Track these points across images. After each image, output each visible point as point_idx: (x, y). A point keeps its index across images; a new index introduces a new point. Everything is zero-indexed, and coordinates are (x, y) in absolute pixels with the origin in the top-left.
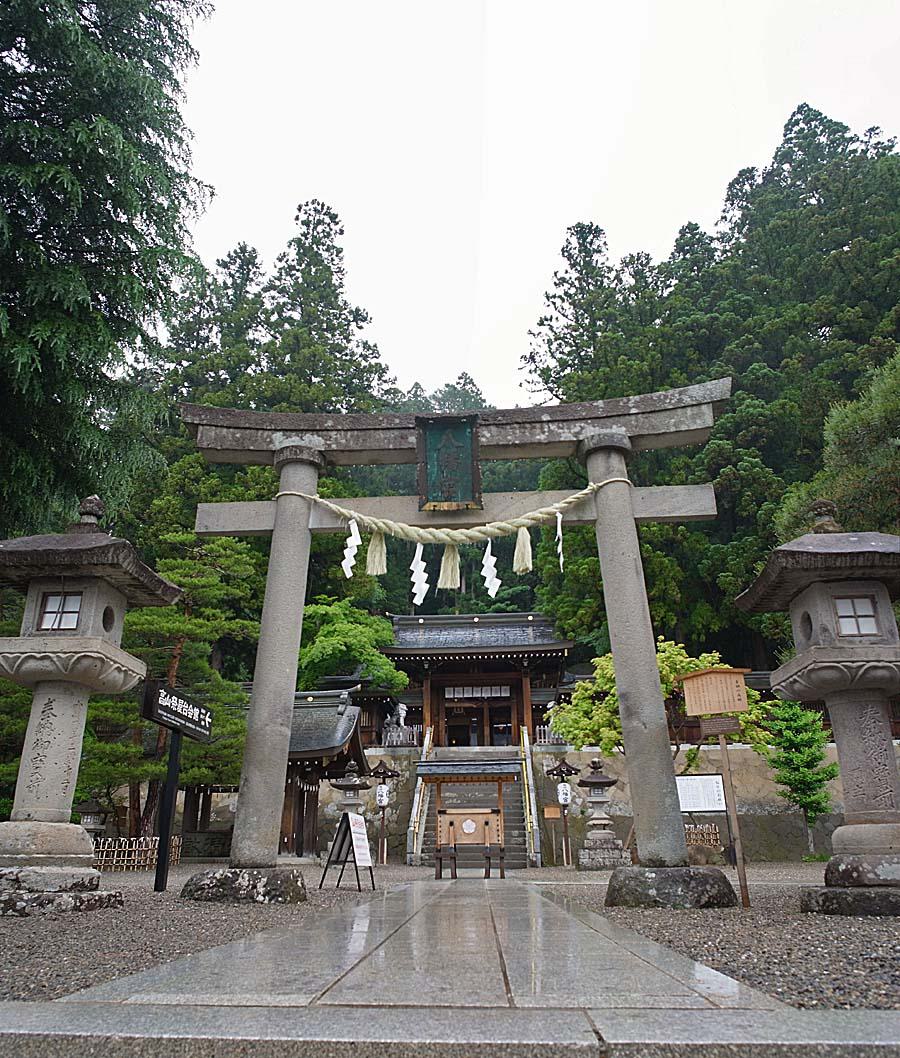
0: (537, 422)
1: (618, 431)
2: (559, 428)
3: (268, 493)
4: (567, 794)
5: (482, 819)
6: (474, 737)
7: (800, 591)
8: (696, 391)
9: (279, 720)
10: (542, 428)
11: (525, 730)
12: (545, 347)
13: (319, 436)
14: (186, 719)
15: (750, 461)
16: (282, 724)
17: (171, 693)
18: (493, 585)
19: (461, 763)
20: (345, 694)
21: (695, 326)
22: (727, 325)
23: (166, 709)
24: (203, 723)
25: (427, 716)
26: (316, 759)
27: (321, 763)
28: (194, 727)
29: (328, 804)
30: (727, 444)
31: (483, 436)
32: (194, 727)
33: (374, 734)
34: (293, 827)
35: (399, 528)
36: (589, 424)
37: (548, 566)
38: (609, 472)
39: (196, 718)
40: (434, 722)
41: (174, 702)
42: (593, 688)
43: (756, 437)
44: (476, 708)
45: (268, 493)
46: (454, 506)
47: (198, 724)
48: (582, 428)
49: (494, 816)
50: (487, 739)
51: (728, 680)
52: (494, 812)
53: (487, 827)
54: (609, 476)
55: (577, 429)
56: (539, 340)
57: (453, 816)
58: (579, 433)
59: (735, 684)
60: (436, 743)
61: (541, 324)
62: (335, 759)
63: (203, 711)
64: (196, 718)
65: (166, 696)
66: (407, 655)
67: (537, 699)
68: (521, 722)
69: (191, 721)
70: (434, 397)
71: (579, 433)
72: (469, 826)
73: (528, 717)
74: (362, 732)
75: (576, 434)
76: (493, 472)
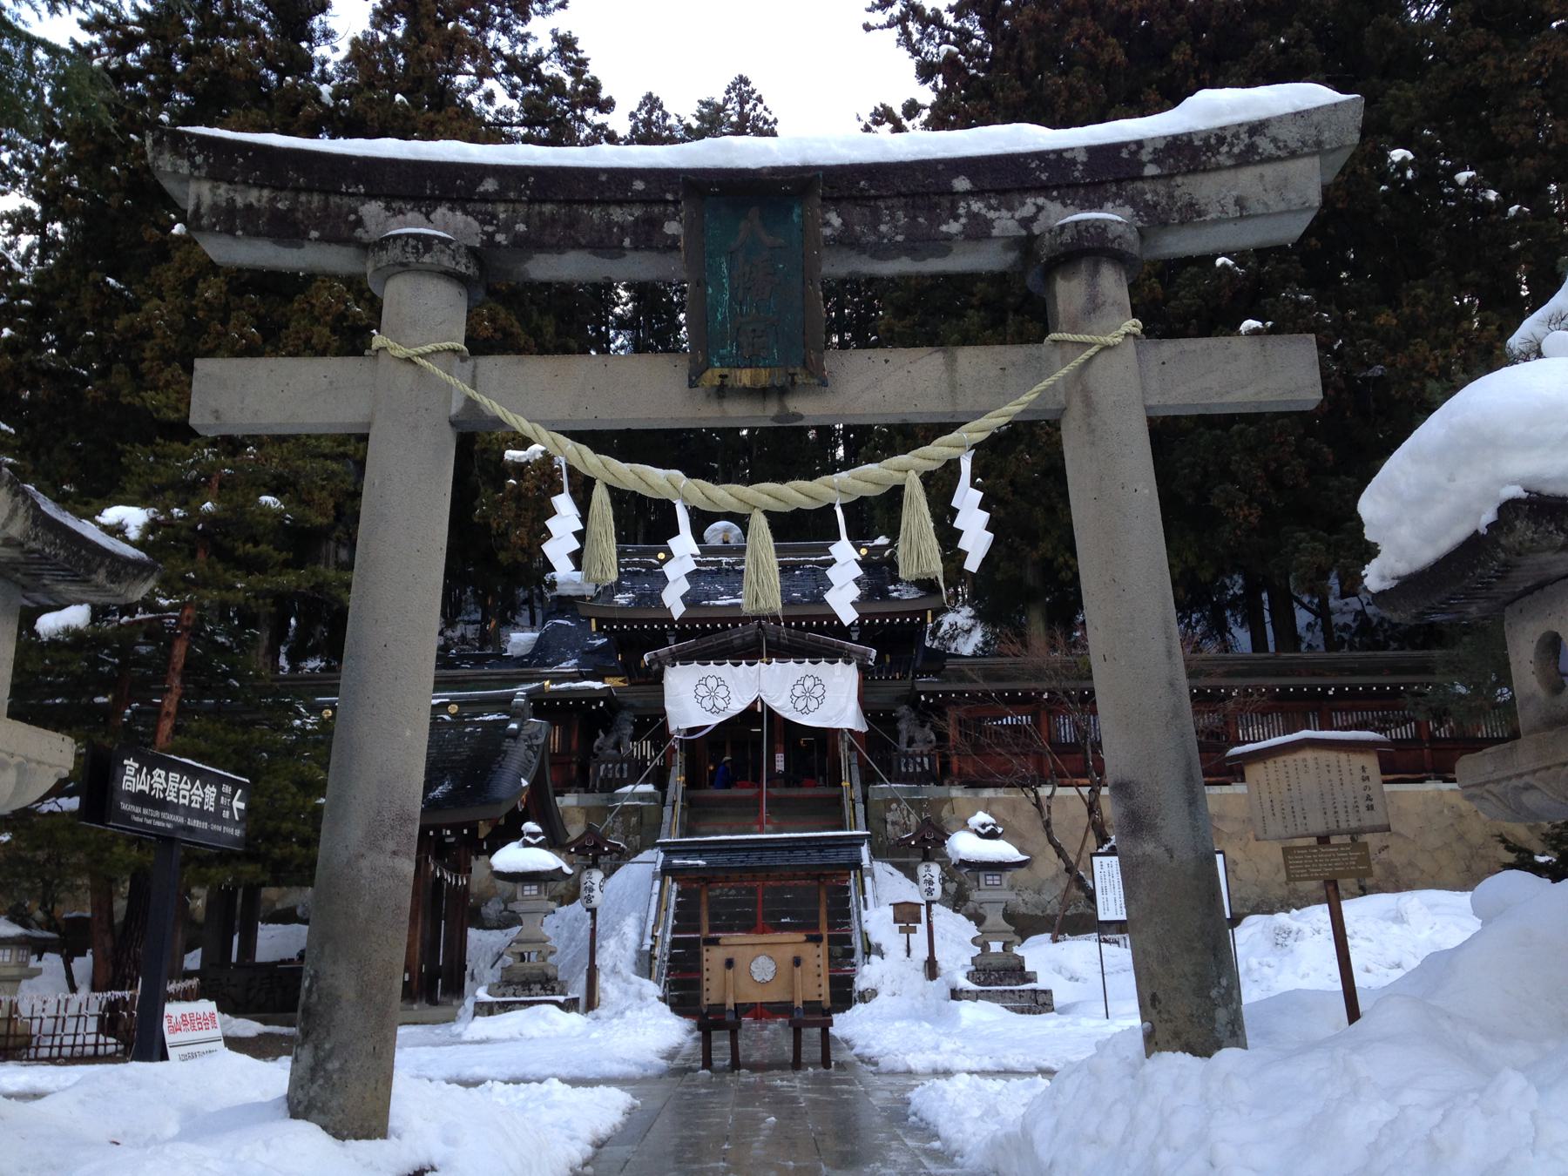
0: (942, 194)
2: (990, 207)
3: (352, 335)
4: (931, 882)
5: (789, 953)
7: (1540, 586)
9: (390, 845)
10: (954, 207)
13: (466, 213)
14: (189, 811)
16: (395, 853)
17: (150, 763)
23: (141, 798)
24: (226, 814)
26: (464, 825)
27: (474, 830)
28: (205, 825)
29: (489, 899)
31: (827, 224)
32: (205, 825)
33: (574, 767)
34: (422, 955)
36: (1053, 199)
37: (273, 77)
38: (1094, 306)
39: (210, 806)
41: (162, 782)
45: (352, 335)
46: (764, 377)
47: (216, 817)
48: (1040, 209)
49: (811, 947)
52: (810, 939)
53: (798, 971)
54: (1100, 325)
55: (1028, 210)
57: (732, 949)
58: (1033, 219)
59: (1358, 774)
62: (502, 822)
63: (227, 789)
64: (210, 806)
65: (139, 771)
66: (635, 621)
69: (202, 814)
71: (1033, 219)
72: (763, 968)
74: (552, 764)
75: (1026, 223)
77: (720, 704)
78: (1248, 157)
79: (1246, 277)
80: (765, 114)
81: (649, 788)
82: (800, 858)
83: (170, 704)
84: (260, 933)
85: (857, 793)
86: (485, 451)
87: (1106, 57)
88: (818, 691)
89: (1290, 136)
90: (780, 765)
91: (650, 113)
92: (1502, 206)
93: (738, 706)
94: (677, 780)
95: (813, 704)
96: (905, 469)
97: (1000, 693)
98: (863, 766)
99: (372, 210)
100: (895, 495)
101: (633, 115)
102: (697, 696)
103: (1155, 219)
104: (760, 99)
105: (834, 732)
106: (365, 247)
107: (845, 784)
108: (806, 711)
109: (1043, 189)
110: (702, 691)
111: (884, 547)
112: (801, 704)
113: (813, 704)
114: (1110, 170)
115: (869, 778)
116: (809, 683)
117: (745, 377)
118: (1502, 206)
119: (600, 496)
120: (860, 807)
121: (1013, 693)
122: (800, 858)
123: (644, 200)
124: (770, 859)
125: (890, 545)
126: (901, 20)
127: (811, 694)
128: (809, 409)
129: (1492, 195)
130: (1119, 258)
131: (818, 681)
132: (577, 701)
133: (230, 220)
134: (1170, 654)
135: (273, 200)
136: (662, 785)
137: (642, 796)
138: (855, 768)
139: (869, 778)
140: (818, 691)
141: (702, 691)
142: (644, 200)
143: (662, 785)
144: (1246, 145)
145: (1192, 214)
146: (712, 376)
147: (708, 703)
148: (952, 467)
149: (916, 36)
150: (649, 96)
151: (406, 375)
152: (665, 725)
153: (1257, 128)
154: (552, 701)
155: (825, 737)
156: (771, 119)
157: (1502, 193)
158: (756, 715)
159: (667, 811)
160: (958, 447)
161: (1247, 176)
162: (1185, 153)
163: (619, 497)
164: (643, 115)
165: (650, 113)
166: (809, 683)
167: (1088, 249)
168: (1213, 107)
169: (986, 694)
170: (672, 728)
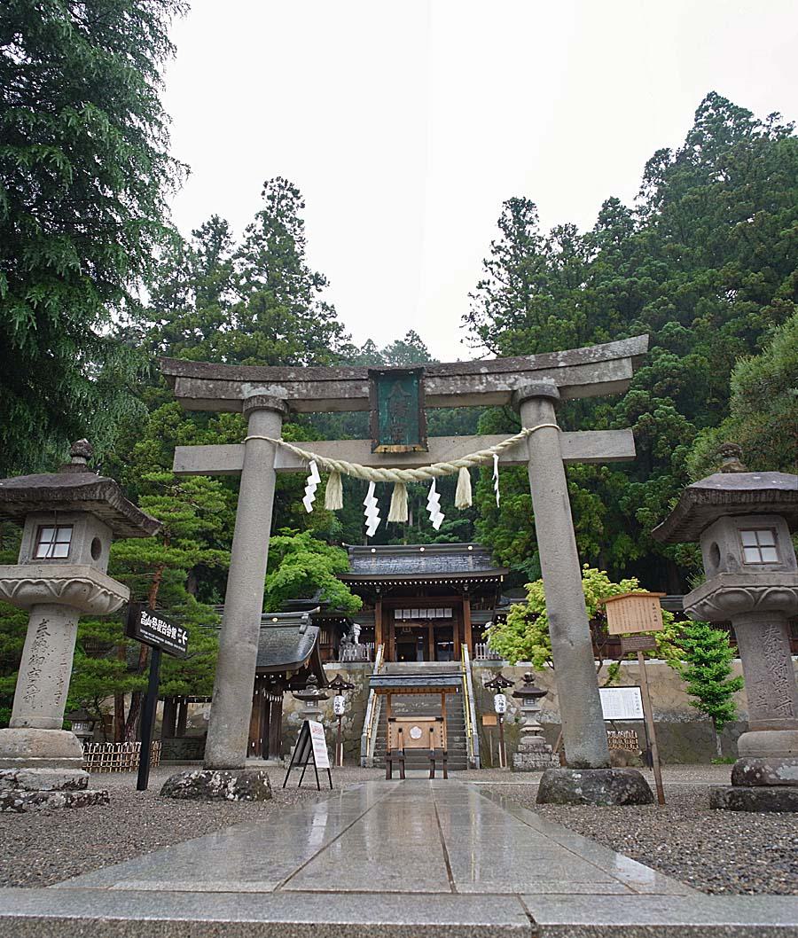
0: (476, 374)
1: (548, 382)
2: (496, 379)
3: (238, 437)
4: (502, 704)
5: (427, 726)
6: (420, 654)
8: (617, 347)
9: (248, 639)
10: (480, 380)
11: (465, 647)
12: (484, 308)
13: (283, 386)
14: (165, 637)
15: (665, 408)
16: (250, 642)
17: (151, 614)
18: (437, 519)
19: (409, 676)
20: (306, 615)
21: (616, 289)
22: (644, 288)
23: (147, 628)
24: (180, 641)
25: (379, 635)
26: (280, 673)
27: (284, 676)
28: (172, 644)
29: (291, 713)
30: (644, 394)
31: (429, 387)
32: (172, 644)
33: (332, 650)
34: (260, 733)
35: (354, 468)
36: (522, 376)
38: (540, 418)
39: (174, 637)
40: (385, 640)
41: (154, 623)
42: (525, 610)
43: (670, 388)
44: (422, 628)
45: (238, 437)
46: (402, 448)
47: (175, 642)
48: (516, 380)
49: (438, 724)
50: (432, 655)
51: (646, 603)
52: (438, 720)
53: (432, 734)
54: (540, 422)
55: (512, 380)
56: (478, 301)
57: (402, 724)
58: (513, 384)
60: (387, 658)
61: (480, 287)
62: (297, 673)
63: (180, 630)
64: (174, 637)
65: (147, 617)
66: (361, 581)
67: (476, 620)
68: (462, 640)
69: (170, 639)
70: (385, 352)
71: (513, 384)
72: (416, 733)
73: (468, 636)
74: (321, 649)
75: (511, 385)
76: (437, 419)
134: (571, 541)
135: (159, 721)
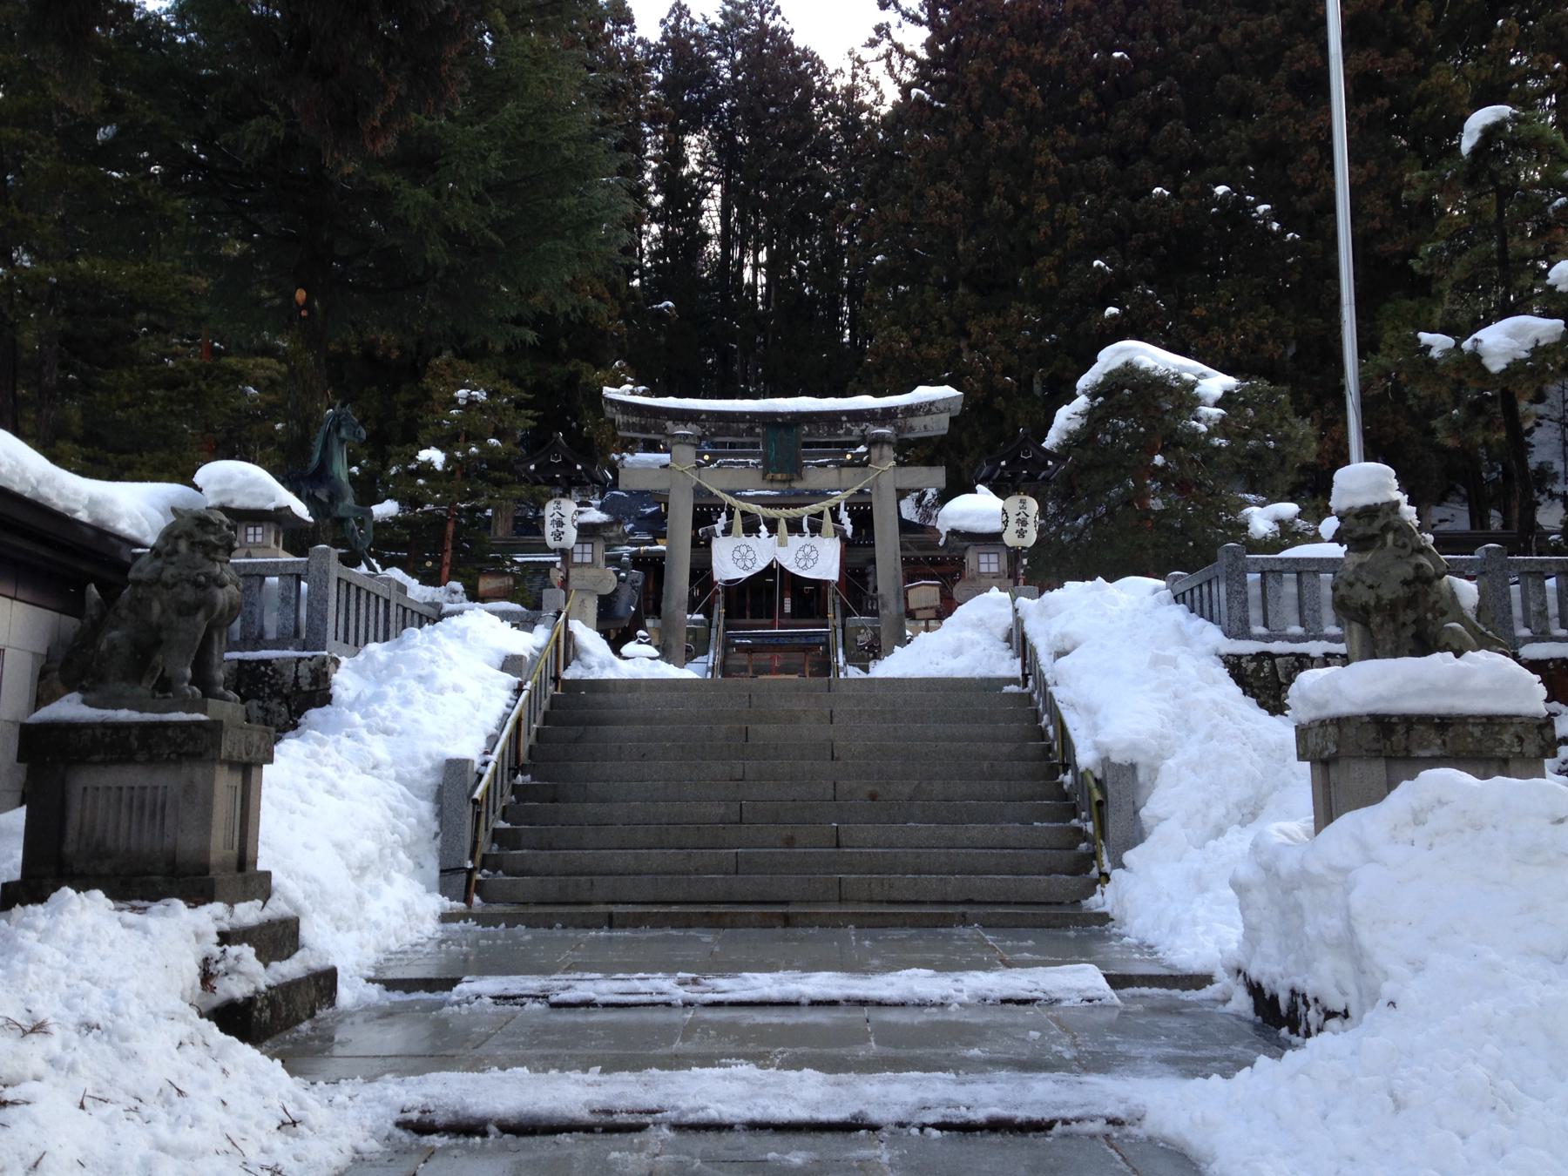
38: (881, 458)
54: (886, 462)
77: (749, 564)
78: (929, 412)
79: (1112, 275)
80: (783, 24)
81: (701, 617)
82: (796, 640)
83: (447, 558)
84: (836, 566)
85: (838, 621)
86: (586, 384)
87: (1029, 101)
88: (814, 555)
89: (941, 407)
90: (788, 609)
91: (678, 19)
92: (1282, 233)
93: (761, 565)
94: (719, 610)
95: (810, 564)
96: (824, 506)
97: (926, 558)
98: (843, 604)
99: (669, 424)
100: (820, 515)
101: (663, 22)
102: (735, 559)
103: (899, 430)
104: (778, 11)
105: (826, 582)
106: (668, 436)
107: (830, 616)
108: (805, 568)
109: (868, 421)
110: (737, 555)
111: (863, 454)
112: (802, 564)
113: (810, 564)
114: (887, 415)
115: (846, 613)
116: (807, 550)
117: (779, 476)
118: (1282, 233)
119: (737, 514)
120: (839, 631)
121: (934, 558)
122: (796, 640)
123: (749, 421)
124: (781, 640)
125: (868, 453)
126: (888, 56)
127: (809, 557)
128: (797, 485)
129: (1275, 226)
130: (889, 443)
131: (813, 548)
132: (653, 559)
133: (628, 427)
136: (709, 615)
137: (696, 622)
138: (838, 607)
139: (846, 613)
140: (814, 555)
141: (737, 555)
142: (749, 421)
143: (709, 615)
144: (928, 408)
145: (911, 429)
146: (769, 476)
147: (741, 564)
148: (838, 506)
149: (897, 69)
150: (678, 4)
151: (681, 476)
152: (711, 576)
153: (932, 403)
154: (645, 559)
155: (820, 585)
156: (788, 29)
157: (1282, 226)
158: (773, 571)
159: (713, 631)
160: (840, 497)
161: (928, 418)
162: (910, 410)
163: (744, 514)
164: (671, 22)
165: (678, 19)
166: (807, 550)
167: (877, 441)
168: (924, 393)
169: (917, 559)
170: (716, 578)
